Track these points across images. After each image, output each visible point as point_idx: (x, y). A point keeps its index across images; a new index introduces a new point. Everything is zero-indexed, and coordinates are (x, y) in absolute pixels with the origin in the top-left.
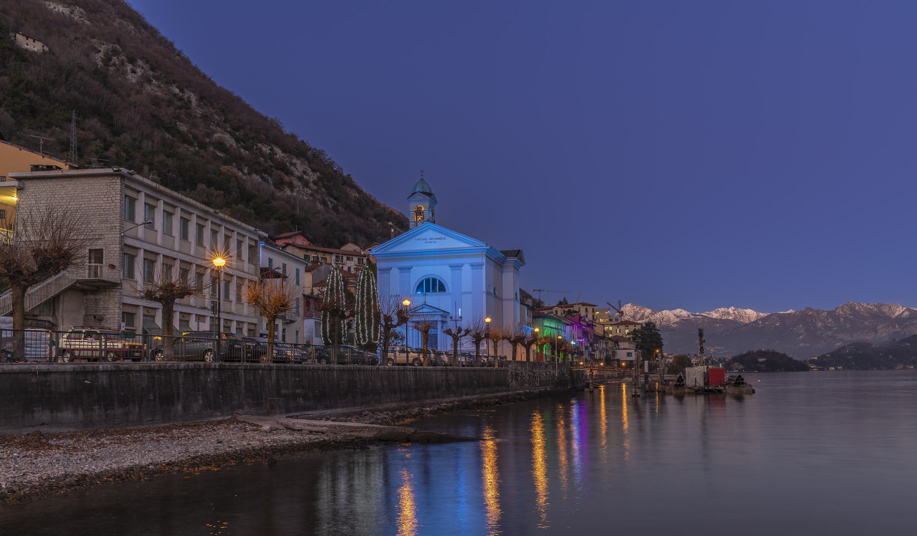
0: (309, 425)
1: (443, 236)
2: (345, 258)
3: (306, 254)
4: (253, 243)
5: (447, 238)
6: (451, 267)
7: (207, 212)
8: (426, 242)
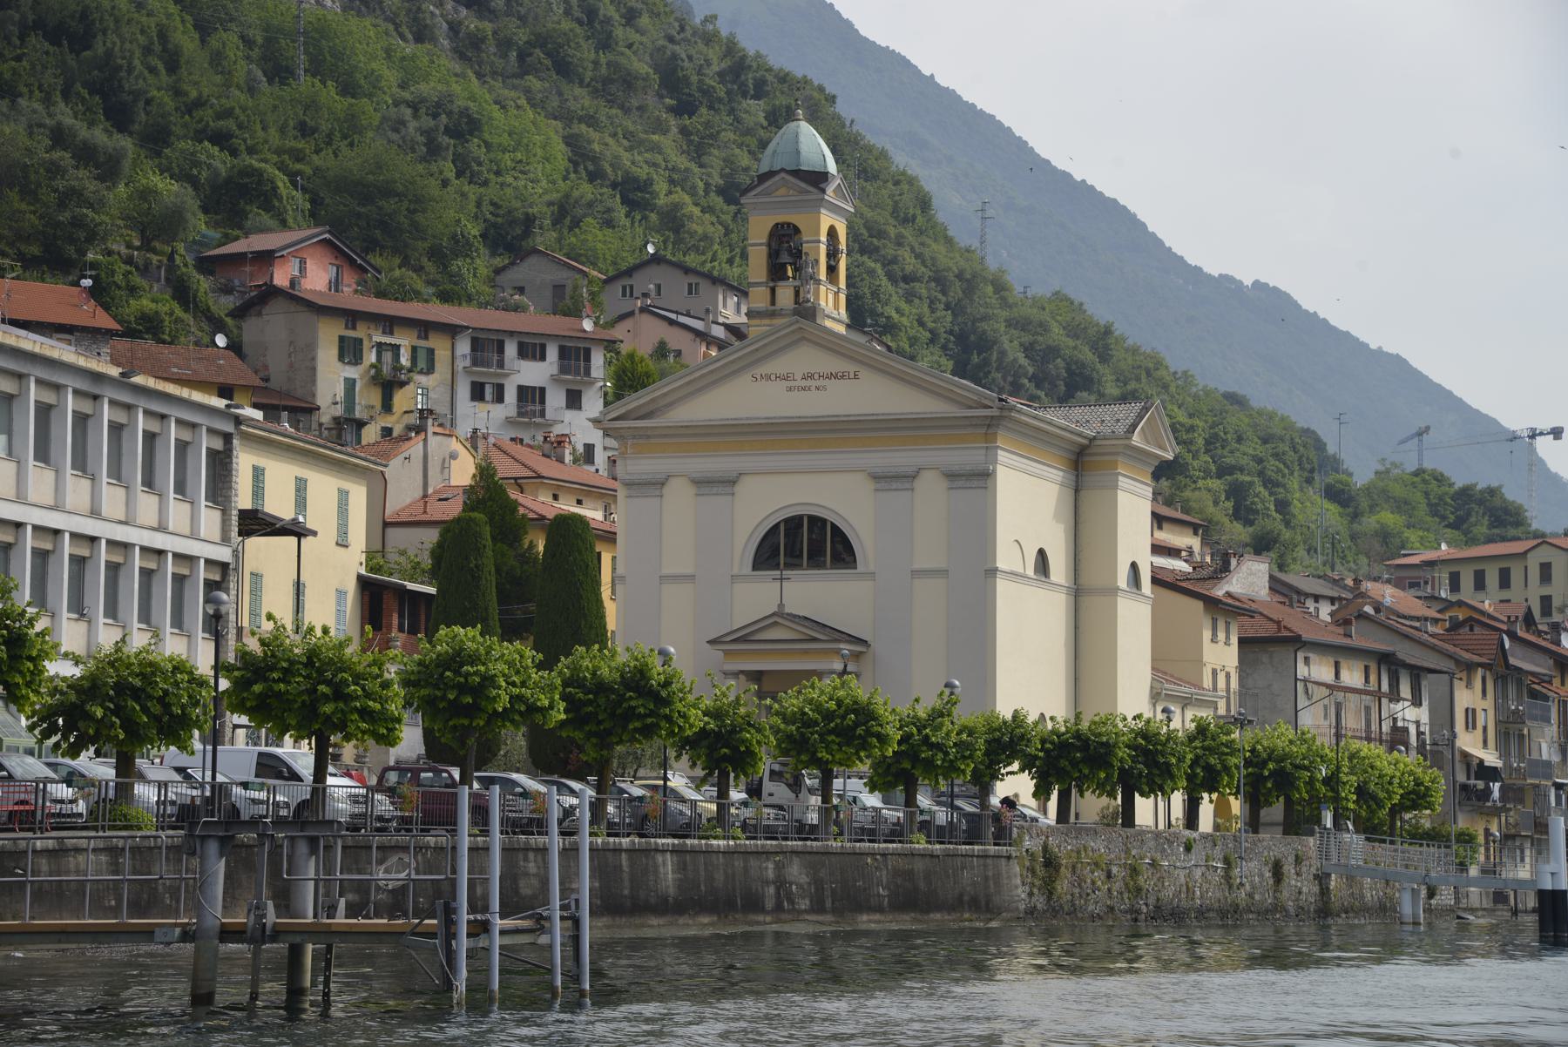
0: (1077, 1035)
1: (851, 368)
2: (511, 349)
3: (351, 333)
4: (218, 444)
5: (865, 374)
6: (876, 477)
7: (98, 377)
8: (790, 389)
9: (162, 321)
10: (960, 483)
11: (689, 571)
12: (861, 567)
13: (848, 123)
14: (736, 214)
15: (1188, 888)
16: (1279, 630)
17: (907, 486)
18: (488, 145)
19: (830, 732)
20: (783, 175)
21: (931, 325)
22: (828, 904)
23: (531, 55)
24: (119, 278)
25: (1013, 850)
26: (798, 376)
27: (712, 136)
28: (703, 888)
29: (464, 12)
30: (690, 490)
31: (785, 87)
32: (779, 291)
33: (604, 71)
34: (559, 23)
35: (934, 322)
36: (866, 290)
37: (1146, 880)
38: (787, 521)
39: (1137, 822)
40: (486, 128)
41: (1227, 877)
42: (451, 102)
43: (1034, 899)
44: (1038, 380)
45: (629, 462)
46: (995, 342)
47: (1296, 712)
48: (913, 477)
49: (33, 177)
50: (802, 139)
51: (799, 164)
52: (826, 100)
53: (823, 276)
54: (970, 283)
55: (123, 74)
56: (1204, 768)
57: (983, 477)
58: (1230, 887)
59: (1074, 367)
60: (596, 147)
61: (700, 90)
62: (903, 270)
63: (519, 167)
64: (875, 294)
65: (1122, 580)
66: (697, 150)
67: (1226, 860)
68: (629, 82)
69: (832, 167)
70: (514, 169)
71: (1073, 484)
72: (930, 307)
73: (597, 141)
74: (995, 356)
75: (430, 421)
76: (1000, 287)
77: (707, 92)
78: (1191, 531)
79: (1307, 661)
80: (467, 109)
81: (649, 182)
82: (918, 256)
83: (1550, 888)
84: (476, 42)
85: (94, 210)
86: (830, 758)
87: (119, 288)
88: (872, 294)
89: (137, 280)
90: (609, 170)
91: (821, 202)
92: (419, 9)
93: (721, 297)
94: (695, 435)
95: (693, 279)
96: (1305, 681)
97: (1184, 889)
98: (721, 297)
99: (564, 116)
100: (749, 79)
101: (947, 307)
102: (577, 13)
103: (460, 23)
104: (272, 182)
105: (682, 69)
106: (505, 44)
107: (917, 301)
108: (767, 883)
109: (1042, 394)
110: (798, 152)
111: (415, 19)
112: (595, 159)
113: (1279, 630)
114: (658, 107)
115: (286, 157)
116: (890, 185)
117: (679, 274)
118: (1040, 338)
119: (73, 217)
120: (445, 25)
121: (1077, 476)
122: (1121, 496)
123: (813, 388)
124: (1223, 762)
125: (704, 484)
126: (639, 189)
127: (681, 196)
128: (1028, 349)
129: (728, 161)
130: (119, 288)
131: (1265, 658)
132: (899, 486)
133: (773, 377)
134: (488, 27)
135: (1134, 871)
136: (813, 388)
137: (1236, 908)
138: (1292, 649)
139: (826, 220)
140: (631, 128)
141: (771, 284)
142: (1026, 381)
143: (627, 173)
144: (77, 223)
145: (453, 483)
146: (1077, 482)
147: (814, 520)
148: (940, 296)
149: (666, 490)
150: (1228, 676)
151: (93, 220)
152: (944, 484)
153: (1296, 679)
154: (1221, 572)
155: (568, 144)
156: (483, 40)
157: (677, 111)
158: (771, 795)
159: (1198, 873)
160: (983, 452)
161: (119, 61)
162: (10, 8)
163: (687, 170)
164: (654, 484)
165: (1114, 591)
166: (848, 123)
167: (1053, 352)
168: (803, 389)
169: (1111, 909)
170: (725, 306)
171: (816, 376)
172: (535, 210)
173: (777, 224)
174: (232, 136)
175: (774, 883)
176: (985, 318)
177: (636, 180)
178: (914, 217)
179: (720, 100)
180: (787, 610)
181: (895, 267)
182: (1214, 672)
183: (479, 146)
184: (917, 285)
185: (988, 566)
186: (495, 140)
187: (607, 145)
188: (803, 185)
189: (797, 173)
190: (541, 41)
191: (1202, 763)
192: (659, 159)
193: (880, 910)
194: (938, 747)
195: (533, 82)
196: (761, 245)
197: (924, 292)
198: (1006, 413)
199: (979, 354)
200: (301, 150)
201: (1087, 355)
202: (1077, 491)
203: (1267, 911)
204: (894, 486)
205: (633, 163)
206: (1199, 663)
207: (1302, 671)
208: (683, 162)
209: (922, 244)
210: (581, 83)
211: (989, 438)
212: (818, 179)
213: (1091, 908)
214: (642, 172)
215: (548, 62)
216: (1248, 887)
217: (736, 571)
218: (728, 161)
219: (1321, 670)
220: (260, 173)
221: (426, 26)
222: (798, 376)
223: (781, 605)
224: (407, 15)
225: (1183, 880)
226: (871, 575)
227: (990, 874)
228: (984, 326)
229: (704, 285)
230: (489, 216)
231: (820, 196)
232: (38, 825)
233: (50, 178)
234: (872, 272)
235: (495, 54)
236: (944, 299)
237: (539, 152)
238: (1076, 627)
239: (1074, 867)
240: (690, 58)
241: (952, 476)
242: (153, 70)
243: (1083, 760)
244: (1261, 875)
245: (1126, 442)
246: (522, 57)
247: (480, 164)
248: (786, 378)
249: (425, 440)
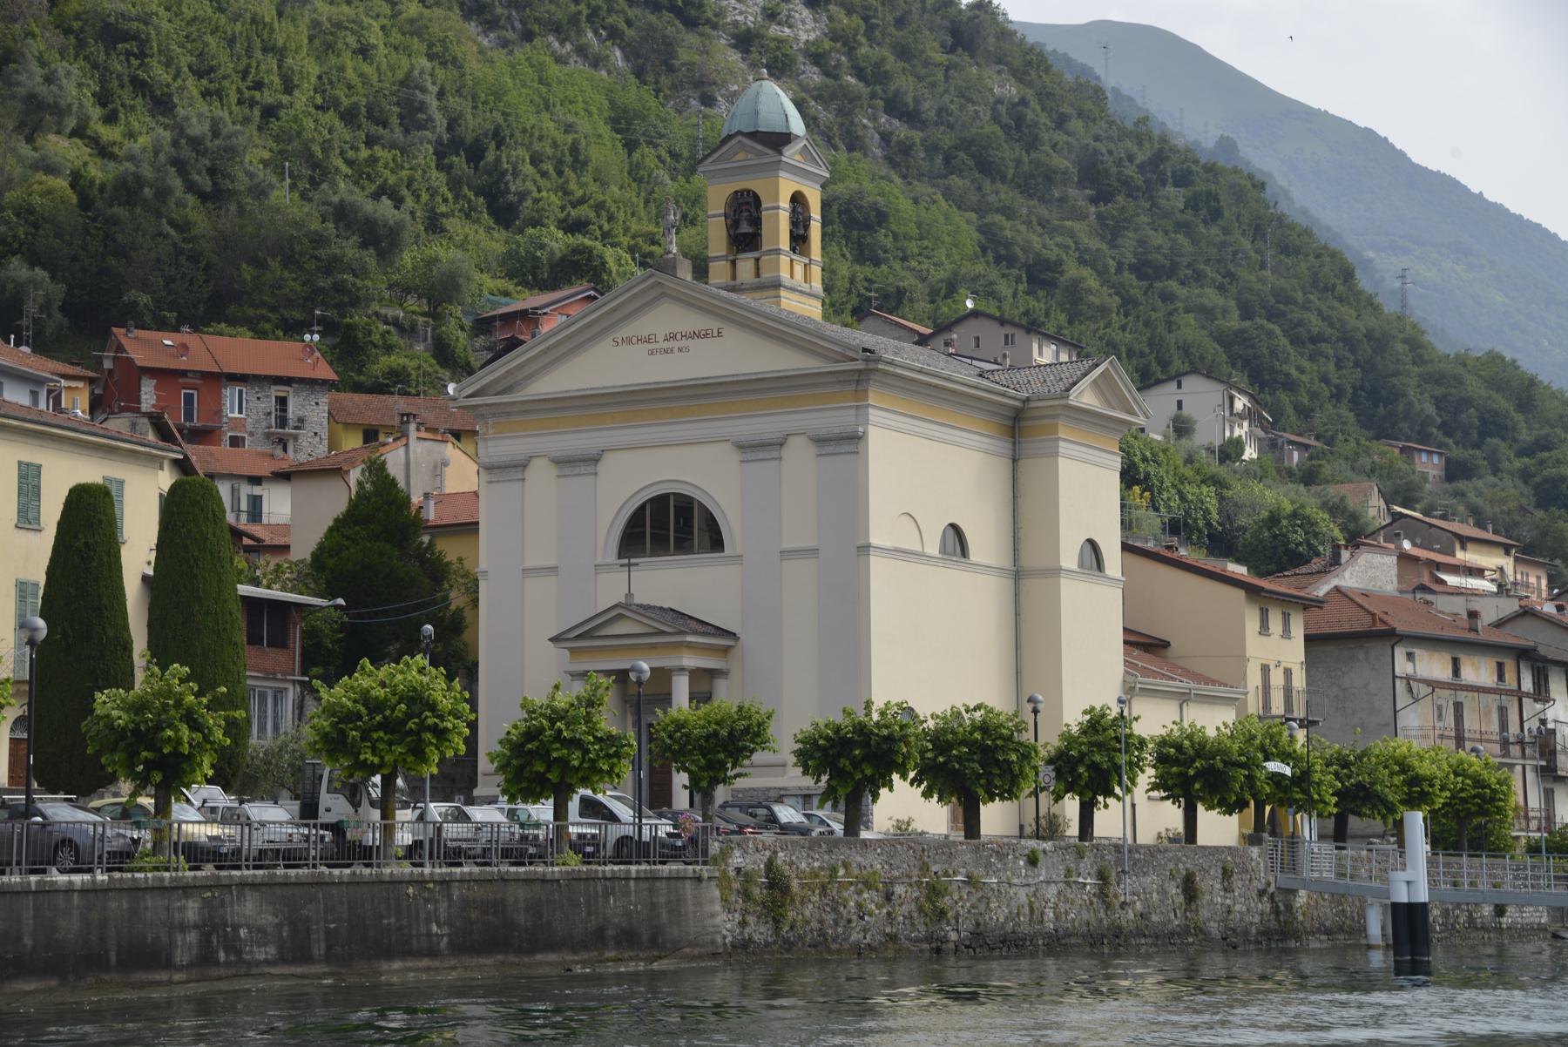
5: (730, 332)
6: (742, 447)
8: (652, 353)
9: (409, 375)
10: (829, 449)
11: (552, 562)
12: (728, 550)
13: (1272, 204)
14: (1148, 289)
15: (1032, 910)
16: (1374, 623)
17: (775, 454)
18: (895, 236)
19: (380, 727)
20: (740, 138)
21: (1336, 381)
22: (319, 949)
23: (956, 157)
24: (376, 338)
25: (705, 871)
26: (660, 338)
27: (1125, 220)
28: (28, 941)
29: (896, 122)
30: (553, 471)
31: (1210, 175)
32: (740, 264)
33: (1026, 168)
34: (982, 128)
35: (1339, 378)
36: (1265, 351)
37: (958, 902)
38: (651, 500)
39: (983, 831)
40: (892, 220)
41: (1102, 894)
42: (862, 198)
43: (747, 930)
44: (1446, 429)
45: (490, 443)
46: (1404, 395)
47: (1395, 712)
48: (780, 444)
49: (297, 248)
50: (762, 98)
51: (756, 125)
52: (1254, 186)
53: (784, 243)
54: (1379, 342)
55: (509, 177)
56: (1089, 768)
57: (853, 440)
58: (1108, 906)
59: (1487, 416)
60: (1008, 233)
61: (1119, 180)
62: (1309, 332)
63: (925, 252)
64: (1273, 353)
65: (1069, 557)
66: (1112, 231)
67: (1102, 876)
68: (1050, 176)
69: (797, 125)
70: (920, 254)
71: (1010, 452)
72: (1336, 365)
73: (1008, 228)
74: (1401, 408)
75: (412, 427)
76: (1416, 345)
77: (1126, 182)
78: (1503, 551)
79: (1410, 656)
80: (875, 203)
81: (1059, 262)
82: (1324, 319)
83: (1405, 900)
84: (906, 149)
85: (355, 275)
86: (376, 760)
87: (376, 346)
88: (1271, 353)
89: (395, 338)
90: (1020, 253)
91: (777, 166)
92: (852, 123)
93: (1035, 346)
94: (556, 409)
95: (1009, 330)
96: (1408, 679)
97: (1026, 910)
98: (1035, 346)
99: (981, 210)
100: (1168, 168)
101: (1357, 364)
102: (1005, 119)
103: (891, 133)
104: (601, 258)
105: (1102, 163)
106: (932, 149)
107: (1322, 360)
108: (184, 928)
109: (1450, 441)
110: (757, 113)
111: (848, 132)
112: (1008, 244)
113: (1374, 623)
114: (1078, 197)
115: (640, 239)
116: (1311, 258)
117: (994, 326)
118: (1453, 391)
119: (335, 284)
120: (877, 136)
121: (1014, 443)
122: (1064, 465)
123: (676, 350)
124: (1111, 760)
125: (566, 463)
126: (1049, 269)
127: (1086, 272)
128: (1439, 403)
129: (1142, 242)
130: (376, 346)
131: (1361, 655)
132: (766, 455)
133: (634, 340)
134: (917, 136)
135: (934, 891)
136: (676, 350)
137: (1117, 932)
138: (1388, 644)
139: (787, 186)
140: (1047, 215)
141: (731, 258)
142: (1435, 431)
143: (1038, 255)
144: (339, 288)
145: (447, 491)
146: (1014, 450)
147: (679, 497)
148: (1348, 355)
149: (529, 473)
150: (1288, 673)
151: (354, 285)
152: (812, 450)
153: (1394, 677)
154: (1331, 565)
155: (982, 233)
156: (911, 147)
157: (1094, 201)
158: (328, 810)
159: (1052, 891)
160: (853, 412)
161: (505, 166)
162: (427, 129)
163: (1098, 250)
164: (514, 466)
165: (1056, 571)
166: (1272, 204)
167: (1467, 402)
168: (666, 351)
169: (893, 938)
170: (1040, 354)
171: (679, 336)
172: (906, 283)
173: (736, 192)
174: (589, 223)
175: (196, 926)
176: (1397, 373)
177: (1047, 261)
178: (1334, 287)
179: (1138, 189)
180: (637, 600)
181: (1301, 329)
182: (1265, 670)
183: (886, 236)
184: (1324, 345)
185: (862, 542)
186: (902, 229)
187: (1018, 231)
188: (759, 147)
189: (754, 135)
190: (966, 145)
191: (1087, 761)
192: (1070, 242)
193: (433, 953)
194: (575, 743)
195: (956, 181)
196: (719, 215)
197: (1331, 352)
198: (872, 366)
199: (1385, 407)
200: (654, 234)
201: (1503, 404)
202: (1015, 460)
203: (1172, 934)
204: (761, 455)
205: (1044, 247)
206: (1242, 659)
207: (1402, 666)
208: (1094, 244)
209: (1331, 308)
210: (1003, 180)
211: (860, 394)
212: (779, 140)
213: (855, 937)
214: (1052, 254)
215: (971, 163)
216: (1139, 906)
217: (599, 561)
218: (1142, 242)
219: (1434, 666)
220: (590, 250)
221: (858, 138)
222: (660, 338)
223: (629, 595)
224: (840, 128)
225: (1023, 899)
226: (738, 558)
227: (662, 900)
228: (1395, 381)
229: (1020, 335)
230: (862, 291)
231: (778, 158)
232: (244, 863)
233: (313, 248)
234: (1270, 334)
235: (923, 159)
236: (1352, 358)
237: (947, 239)
238: (1017, 614)
239: (824, 888)
240: (1110, 152)
241: (820, 441)
242: (544, 174)
243: (865, 758)
244: (1163, 892)
245: (1062, 402)
246: (948, 160)
247: (886, 252)
248: (648, 341)
249: (407, 445)
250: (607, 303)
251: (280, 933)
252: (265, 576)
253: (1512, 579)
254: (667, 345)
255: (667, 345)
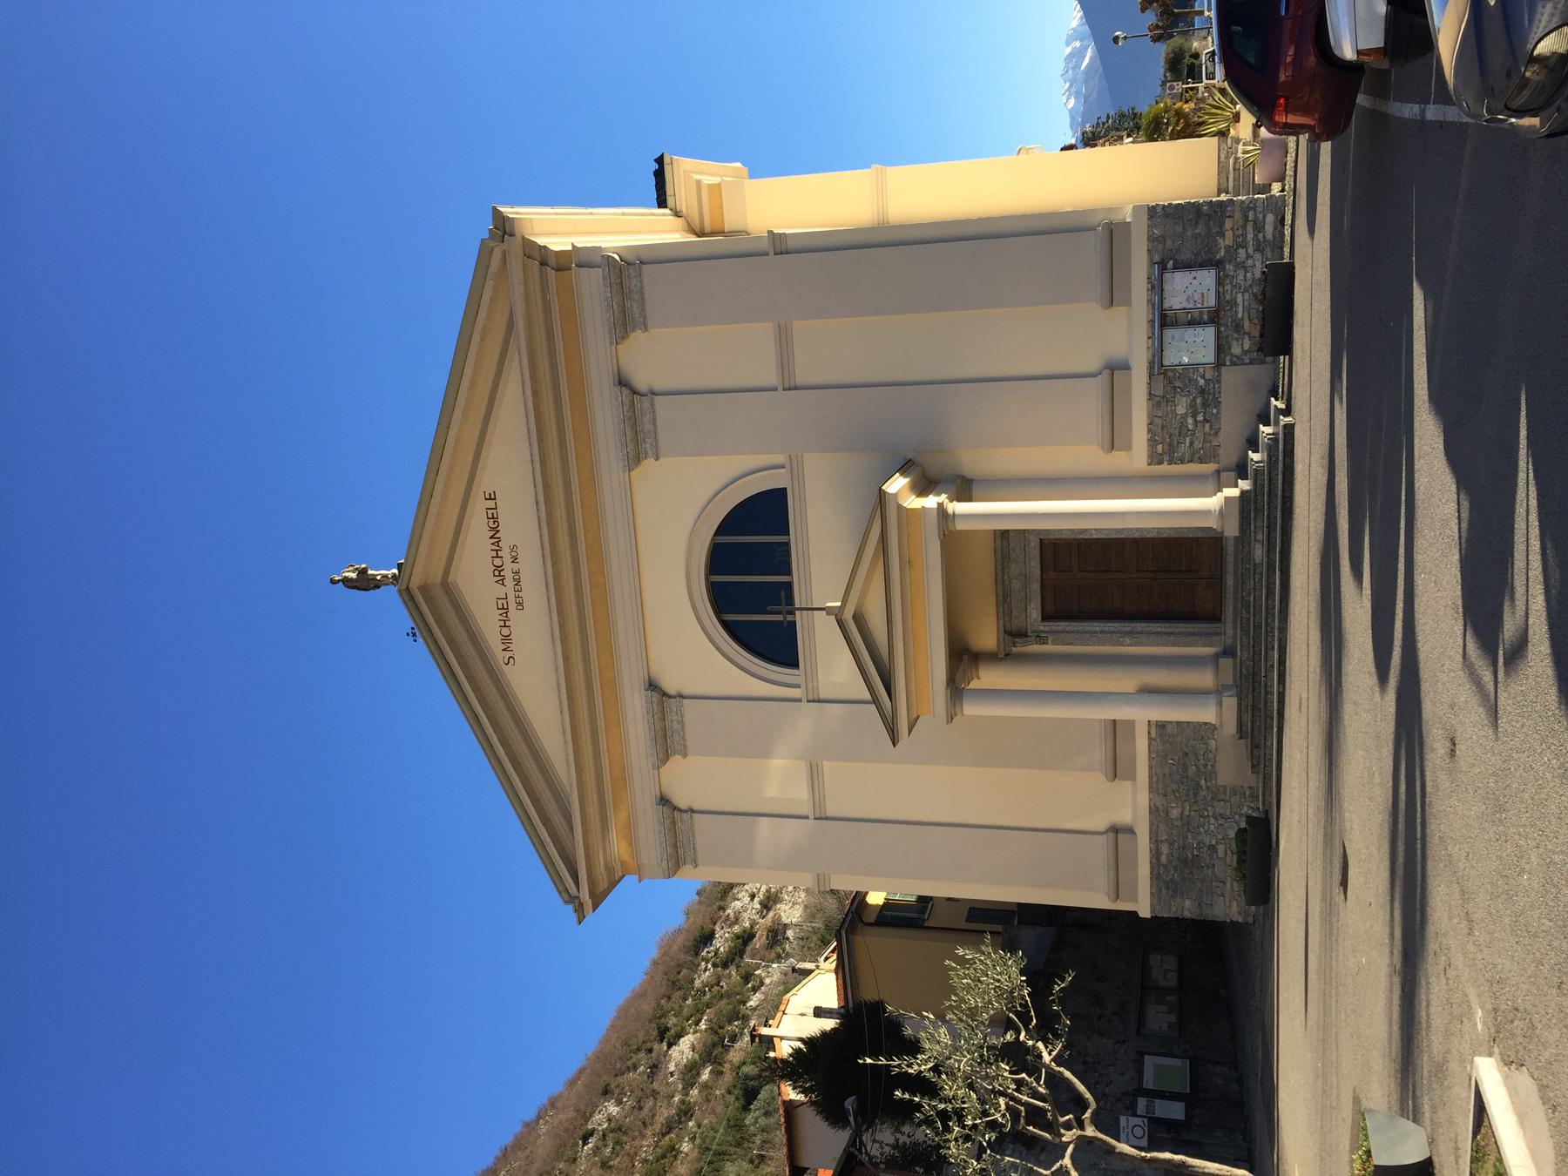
8: (520, 604)
26: (500, 591)
123: (515, 567)
133: (505, 631)
136: (515, 567)
168: (518, 582)
171: (498, 562)
222: (500, 591)
248: (505, 610)
250: (643, 690)
251: (1185, 768)
252: (986, 1008)
253: (1188, 813)
254: (509, 581)
255: (509, 581)
